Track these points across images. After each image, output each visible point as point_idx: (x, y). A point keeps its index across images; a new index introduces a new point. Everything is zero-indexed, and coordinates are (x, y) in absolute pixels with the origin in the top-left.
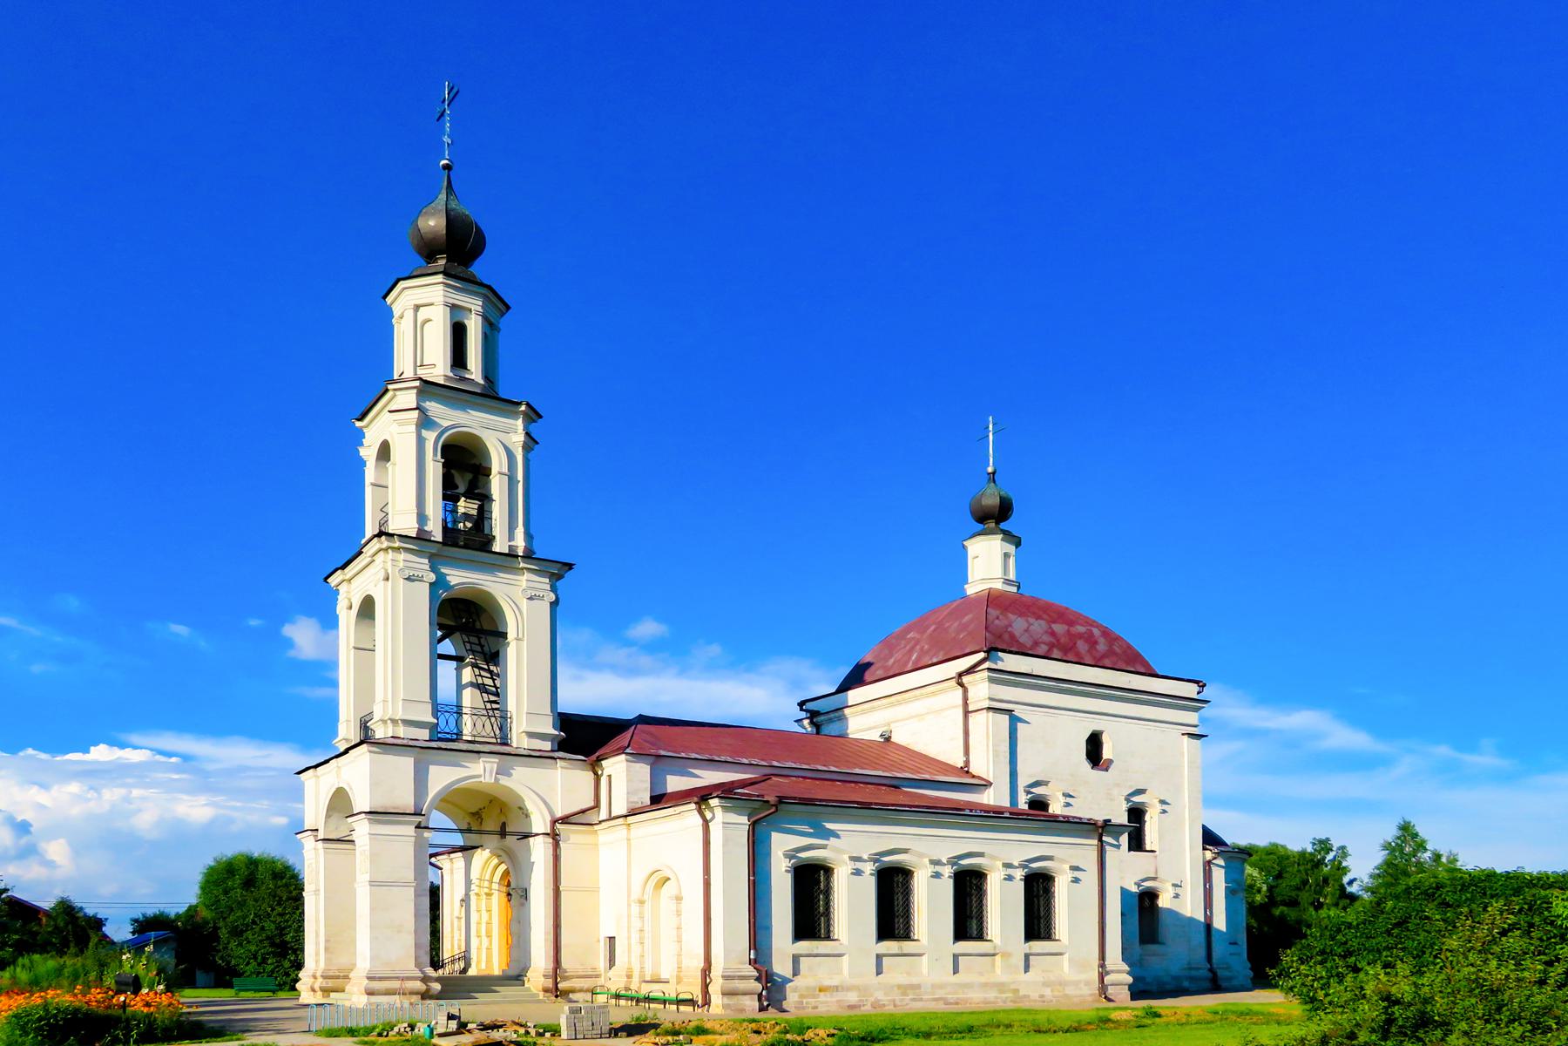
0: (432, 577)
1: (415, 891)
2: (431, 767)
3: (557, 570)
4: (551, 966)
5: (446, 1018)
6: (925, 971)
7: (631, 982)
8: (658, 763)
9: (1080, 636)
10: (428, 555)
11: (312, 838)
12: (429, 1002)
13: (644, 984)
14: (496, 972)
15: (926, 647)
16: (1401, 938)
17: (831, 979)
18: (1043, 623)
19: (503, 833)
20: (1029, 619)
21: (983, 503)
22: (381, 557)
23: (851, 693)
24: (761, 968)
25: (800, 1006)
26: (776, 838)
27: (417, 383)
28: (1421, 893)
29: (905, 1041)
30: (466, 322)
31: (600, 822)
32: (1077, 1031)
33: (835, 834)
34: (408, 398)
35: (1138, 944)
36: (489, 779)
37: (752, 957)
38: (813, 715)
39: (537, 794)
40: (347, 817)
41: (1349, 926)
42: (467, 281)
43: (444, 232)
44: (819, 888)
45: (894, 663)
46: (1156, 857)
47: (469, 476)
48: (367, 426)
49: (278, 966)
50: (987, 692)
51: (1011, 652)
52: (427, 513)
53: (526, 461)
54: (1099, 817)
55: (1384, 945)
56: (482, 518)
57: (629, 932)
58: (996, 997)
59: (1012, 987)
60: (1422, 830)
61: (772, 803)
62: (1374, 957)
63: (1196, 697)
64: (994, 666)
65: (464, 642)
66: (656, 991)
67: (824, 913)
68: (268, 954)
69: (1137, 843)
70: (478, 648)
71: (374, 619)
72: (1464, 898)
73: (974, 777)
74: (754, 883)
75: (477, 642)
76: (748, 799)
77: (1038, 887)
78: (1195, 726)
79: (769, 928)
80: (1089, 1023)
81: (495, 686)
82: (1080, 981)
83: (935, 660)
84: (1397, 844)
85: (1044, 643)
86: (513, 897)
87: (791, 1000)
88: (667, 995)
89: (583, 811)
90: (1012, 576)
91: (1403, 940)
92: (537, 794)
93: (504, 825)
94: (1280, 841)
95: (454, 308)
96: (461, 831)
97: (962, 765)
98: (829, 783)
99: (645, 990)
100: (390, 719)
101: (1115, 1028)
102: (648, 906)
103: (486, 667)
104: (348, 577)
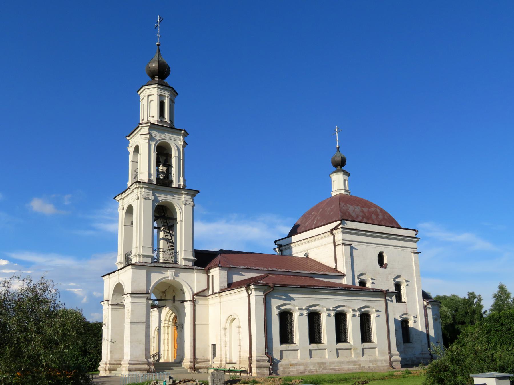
0: (153, 198)
1: (146, 326)
2: (152, 274)
3: (193, 193)
4: (192, 357)
5: (169, 378)
6: (327, 356)
7: (222, 364)
8: (230, 270)
9: (373, 212)
10: (152, 189)
11: (107, 304)
13: (227, 364)
14: (171, 360)
15: (319, 218)
16: (489, 338)
17: (294, 360)
18: (359, 207)
19: (174, 300)
20: (355, 206)
21: (336, 160)
22: (136, 190)
24: (270, 357)
25: (283, 372)
26: (273, 301)
27: (149, 125)
29: (325, 384)
30: (164, 100)
32: (382, 379)
33: (292, 299)
34: (146, 130)
35: (403, 343)
37: (266, 352)
38: (280, 246)
39: (187, 283)
40: (122, 295)
42: (163, 85)
43: (158, 69)
44: (288, 322)
45: (308, 224)
46: (406, 305)
47: (165, 158)
48: (130, 139)
50: (342, 237)
51: (349, 221)
52: (151, 173)
53: (183, 150)
54: (384, 289)
56: (168, 174)
57: (221, 342)
58: (353, 368)
59: (358, 363)
61: (272, 287)
63: (415, 236)
64: (343, 227)
65: (162, 222)
66: (231, 367)
67: (290, 332)
69: (399, 299)
70: (166, 224)
72: (508, 321)
73: (339, 272)
74: (266, 320)
78: (416, 248)
79: (272, 339)
80: (386, 376)
81: (172, 239)
82: (382, 360)
83: (322, 224)
84: (499, 295)
85: (360, 216)
86: (178, 327)
87: (280, 370)
88: (236, 369)
89: (203, 291)
90: (347, 188)
91: (490, 339)
92: (187, 283)
93: (174, 297)
96: (158, 300)
98: (289, 276)
99: (227, 367)
101: (396, 378)
102: (227, 330)
103: (168, 231)
104: (123, 197)
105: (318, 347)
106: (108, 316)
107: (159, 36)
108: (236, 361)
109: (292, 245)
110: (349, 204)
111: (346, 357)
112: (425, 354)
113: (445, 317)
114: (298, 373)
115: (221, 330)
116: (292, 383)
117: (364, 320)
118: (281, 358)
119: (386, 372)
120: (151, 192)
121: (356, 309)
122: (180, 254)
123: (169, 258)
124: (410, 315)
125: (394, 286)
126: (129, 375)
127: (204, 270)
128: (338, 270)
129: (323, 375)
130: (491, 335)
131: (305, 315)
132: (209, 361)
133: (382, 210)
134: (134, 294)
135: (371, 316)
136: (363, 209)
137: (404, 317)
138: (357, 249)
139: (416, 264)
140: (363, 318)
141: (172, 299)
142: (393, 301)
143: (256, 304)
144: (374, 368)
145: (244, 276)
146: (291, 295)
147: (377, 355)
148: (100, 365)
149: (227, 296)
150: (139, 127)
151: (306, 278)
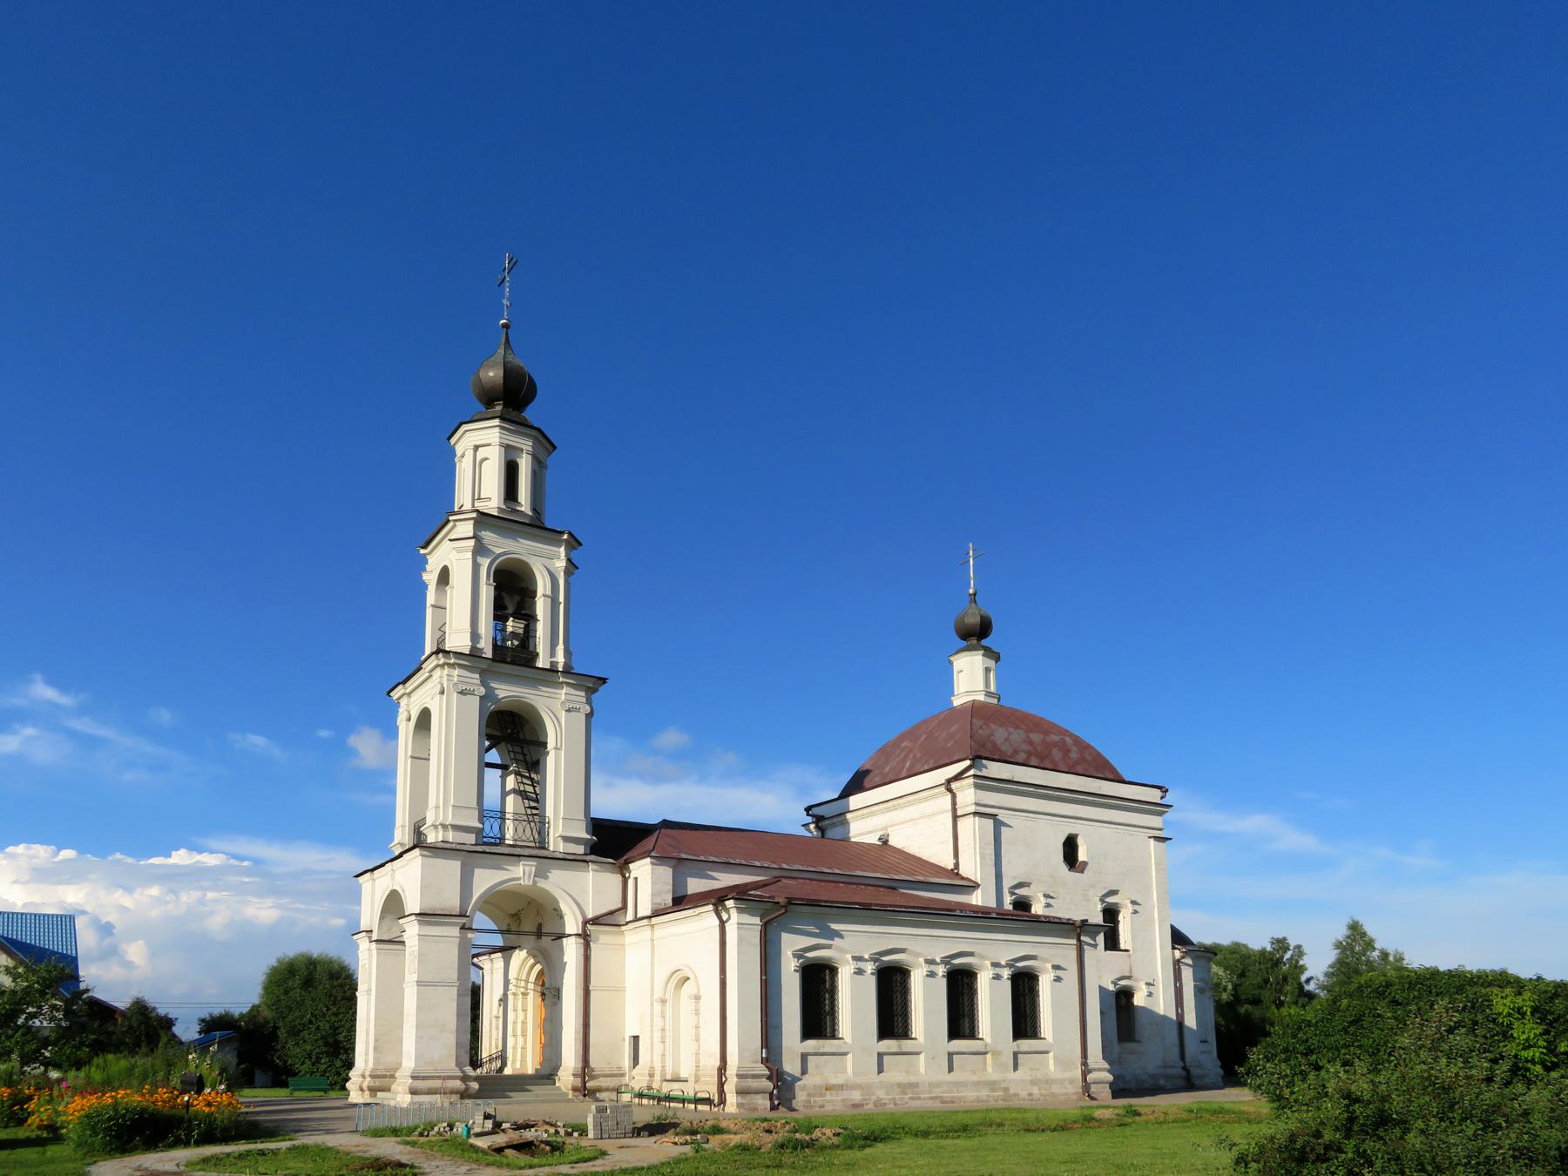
0: (482, 691)
3: (592, 684)
4: (580, 1065)
5: (482, 1117)
6: (922, 1070)
7: (653, 1081)
8: (680, 864)
9: (1055, 744)
12: (467, 1101)
13: (664, 1083)
14: (530, 1071)
15: (918, 755)
17: (836, 1077)
19: (539, 934)
21: (966, 622)
22: (438, 673)
25: (808, 1105)
26: (787, 938)
27: (474, 515)
30: (518, 460)
32: (1063, 1129)
33: (838, 935)
34: (466, 529)
36: (527, 882)
37: (764, 1055)
38: (819, 820)
40: (399, 919)
41: (1309, 1024)
43: (502, 382)
44: (825, 987)
45: (890, 769)
46: (1129, 956)
47: (517, 598)
49: (330, 1066)
50: (973, 797)
51: (993, 760)
52: (479, 632)
54: (1077, 917)
56: (528, 636)
57: (652, 1031)
58: (988, 1096)
59: (1003, 1085)
60: (1371, 929)
63: (1159, 802)
64: (979, 773)
65: (509, 752)
66: (675, 1089)
69: (1112, 943)
70: (521, 757)
71: (429, 730)
72: (1412, 996)
73: (963, 878)
77: (1024, 986)
78: (1161, 830)
79: (779, 1027)
80: (1075, 1122)
81: (535, 793)
82: (1065, 1080)
83: (926, 768)
85: (1023, 751)
88: (686, 1094)
89: (612, 913)
90: (993, 689)
92: (570, 896)
93: (540, 925)
95: (508, 448)
96: (502, 932)
97: (952, 867)
99: (666, 1088)
101: (1099, 1127)
103: (527, 775)
104: (408, 691)
105: (900, 1046)
106: (370, 968)
107: (508, 303)
108: (687, 1076)
109: (849, 816)
110: (995, 724)
111: (972, 1071)
112: (1173, 1067)
113: (1217, 986)
114: (846, 1106)
115: (652, 1004)
116: (811, 1139)
117: (1021, 987)
118: (804, 1071)
119: (1073, 1109)
120: (477, 676)
121: (1003, 963)
122: (552, 827)
123: (528, 834)
124: (1137, 980)
125: (1101, 914)
126: (413, 1103)
127: (613, 866)
128: (960, 872)
129: (907, 1114)
130: (1363, 1028)
131: (869, 972)
132: (623, 1075)
133: (1077, 741)
134: (424, 916)
135: (1040, 978)
136: (1031, 735)
137: (1123, 983)
138: (1011, 827)
139: (1157, 864)
140: (1020, 982)
141: (535, 930)
142: (1097, 945)
143: (739, 945)
144: (1042, 1098)
145: (717, 879)
146: (834, 926)
147: (1052, 1067)
148: (350, 1079)
149: (668, 924)
150: (448, 521)
151: (879, 889)
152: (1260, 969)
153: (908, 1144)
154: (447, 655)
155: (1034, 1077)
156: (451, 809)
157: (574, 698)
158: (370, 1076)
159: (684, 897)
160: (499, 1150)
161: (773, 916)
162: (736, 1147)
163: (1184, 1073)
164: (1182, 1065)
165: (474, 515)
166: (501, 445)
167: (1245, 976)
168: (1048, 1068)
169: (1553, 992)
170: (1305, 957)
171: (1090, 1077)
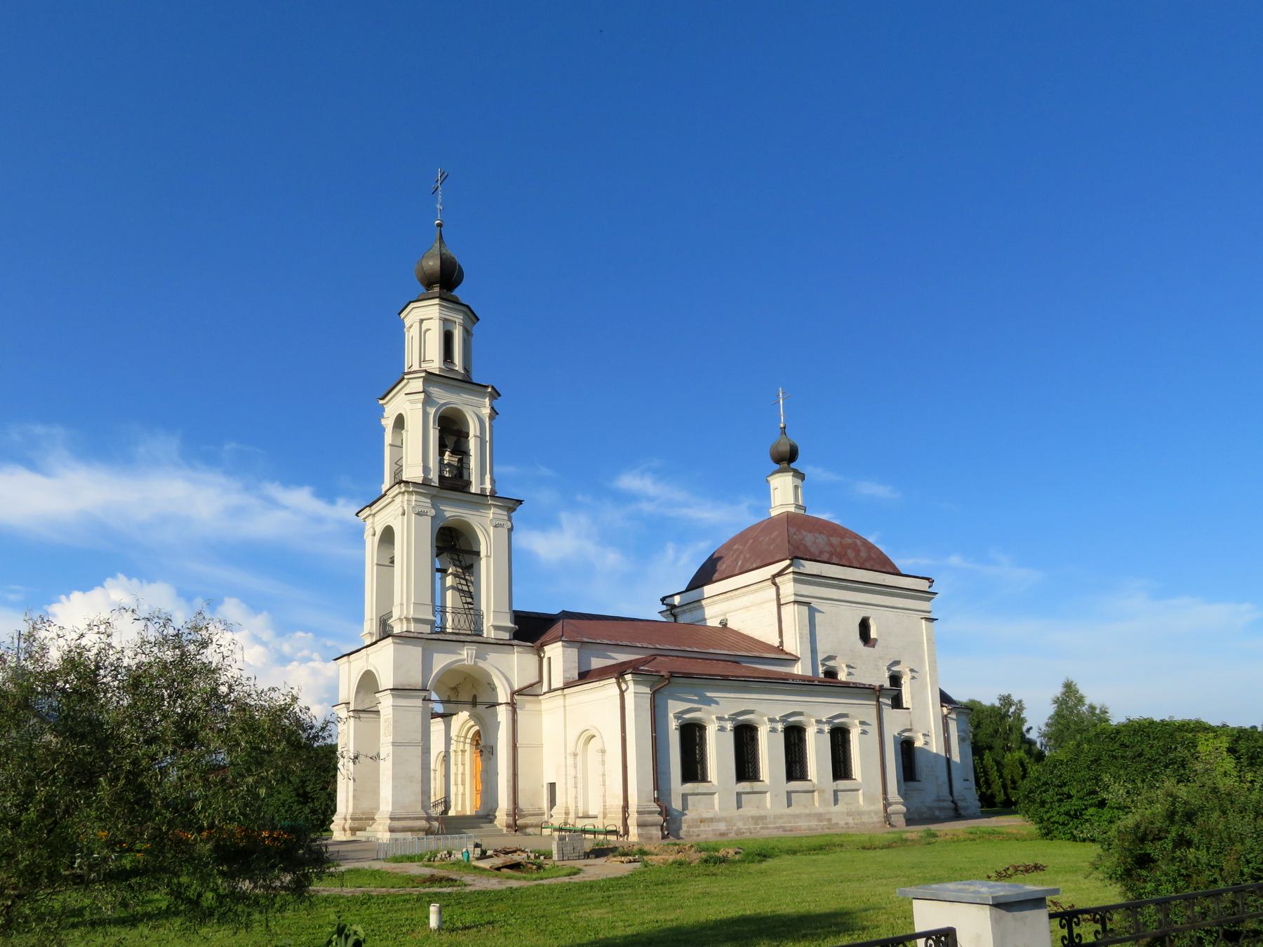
0: (433, 512)
3: (512, 505)
4: (511, 807)
6: (769, 805)
11: (345, 709)
12: (430, 836)
13: (578, 820)
14: (468, 812)
15: (748, 556)
17: (707, 812)
19: (474, 703)
22: (399, 498)
23: (707, 589)
27: (423, 374)
28: (1106, 737)
31: (545, 693)
34: (417, 385)
36: (470, 662)
41: (1061, 762)
43: (439, 269)
46: (910, 713)
49: (300, 813)
53: (490, 424)
54: (877, 684)
55: (1087, 777)
57: (566, 779)
58: (817, 825)
59: (827, 816)
60: (1083, 689)
61: (666, 677)
62: (1081, 786)
64: (797, 570)
68: (293, 803)
69: (897, 703)
70: (457, 563)
71: (394, 544)
72: (1136, 741)
73: (787, 653)
75: (457, 558)
76: (648, 674)
77: (839, 737)
78: (929, 612)
82: (872, 811)
83: (754, 566)
85: (826, 552)
89: (531, 686)
92: (500, 671)
93: (475, 697)
94: (977, 698)
95: (445, 321)
96: (442, 702)
97: (778, 645)
98: (709, 661)
99: (580, 824)
100: (405, 618)
102: (579, 758)
104: (373, 512)
105: (752, 787)
110: (805, 531)
115: (566, 758)
121: (824, 720)
124: (917, 732)
125: (888, 680)
132: (543, 814)
134: (397, 691)
136: (831, 539)
137: (906, 734)
148: (333, 821)
150: (403, 379)
152: (991, 721)
153: (786, 861)
154: (407, 485)
155: (849, 810)
156: (412, 606)
157: (499, 517)
158: (351, 818)
159: (588, 672)
160: (498, 869)
161: (659, 686)
162: (674, 862)
163: (953, 805)
164: (951, 799)
165: (423, 374)
166: (440, 319)
167: (980, 727)
168: (858, 802)
169: (1237, 735)
170: (1024, 711)
171: (890, 809)
